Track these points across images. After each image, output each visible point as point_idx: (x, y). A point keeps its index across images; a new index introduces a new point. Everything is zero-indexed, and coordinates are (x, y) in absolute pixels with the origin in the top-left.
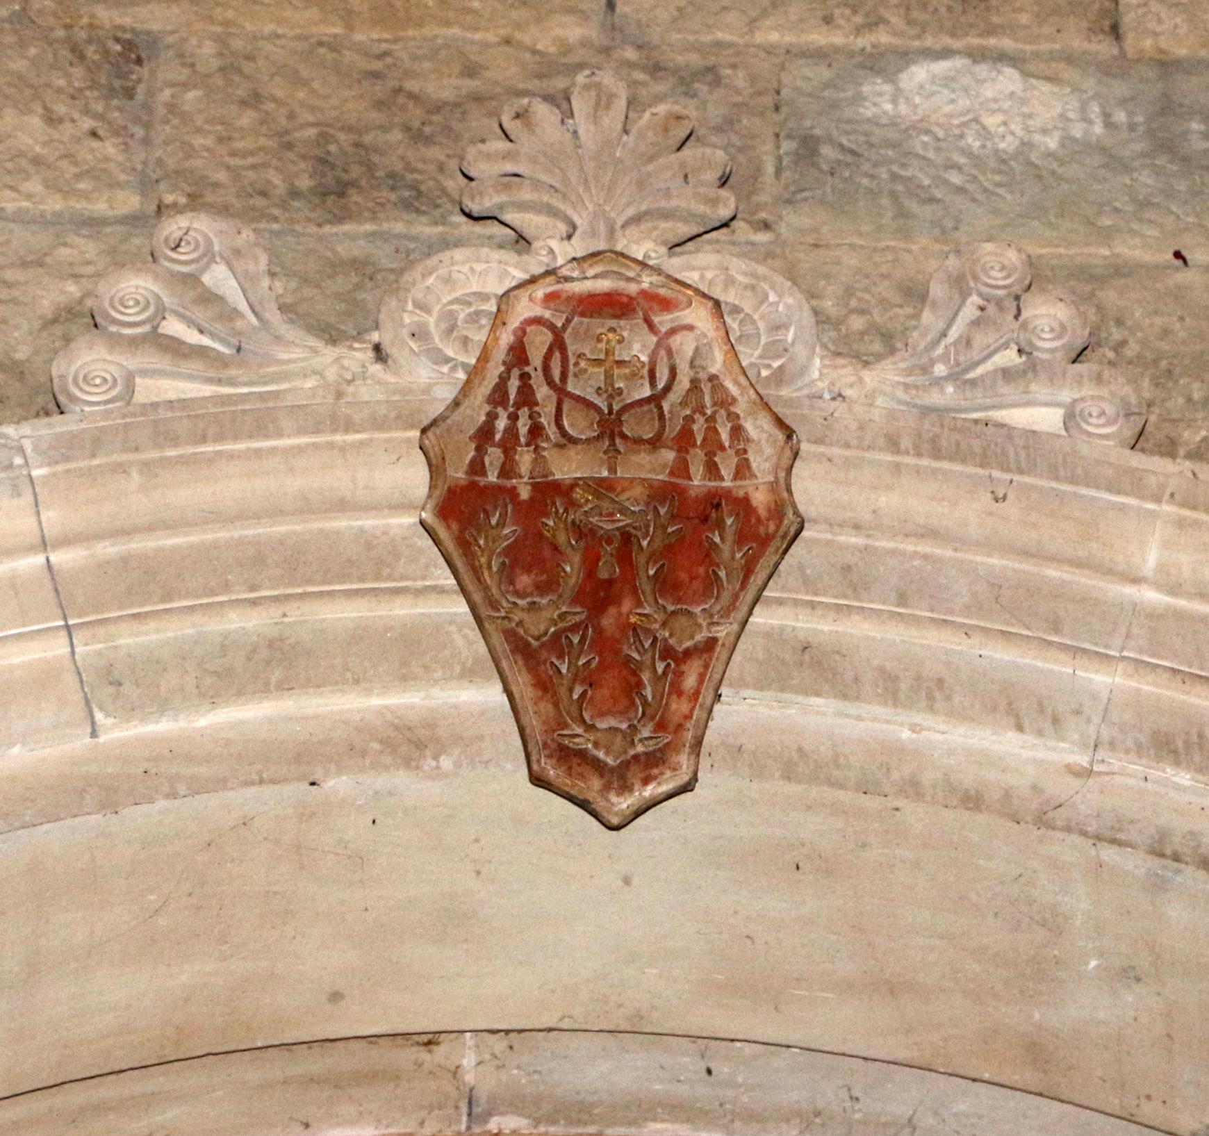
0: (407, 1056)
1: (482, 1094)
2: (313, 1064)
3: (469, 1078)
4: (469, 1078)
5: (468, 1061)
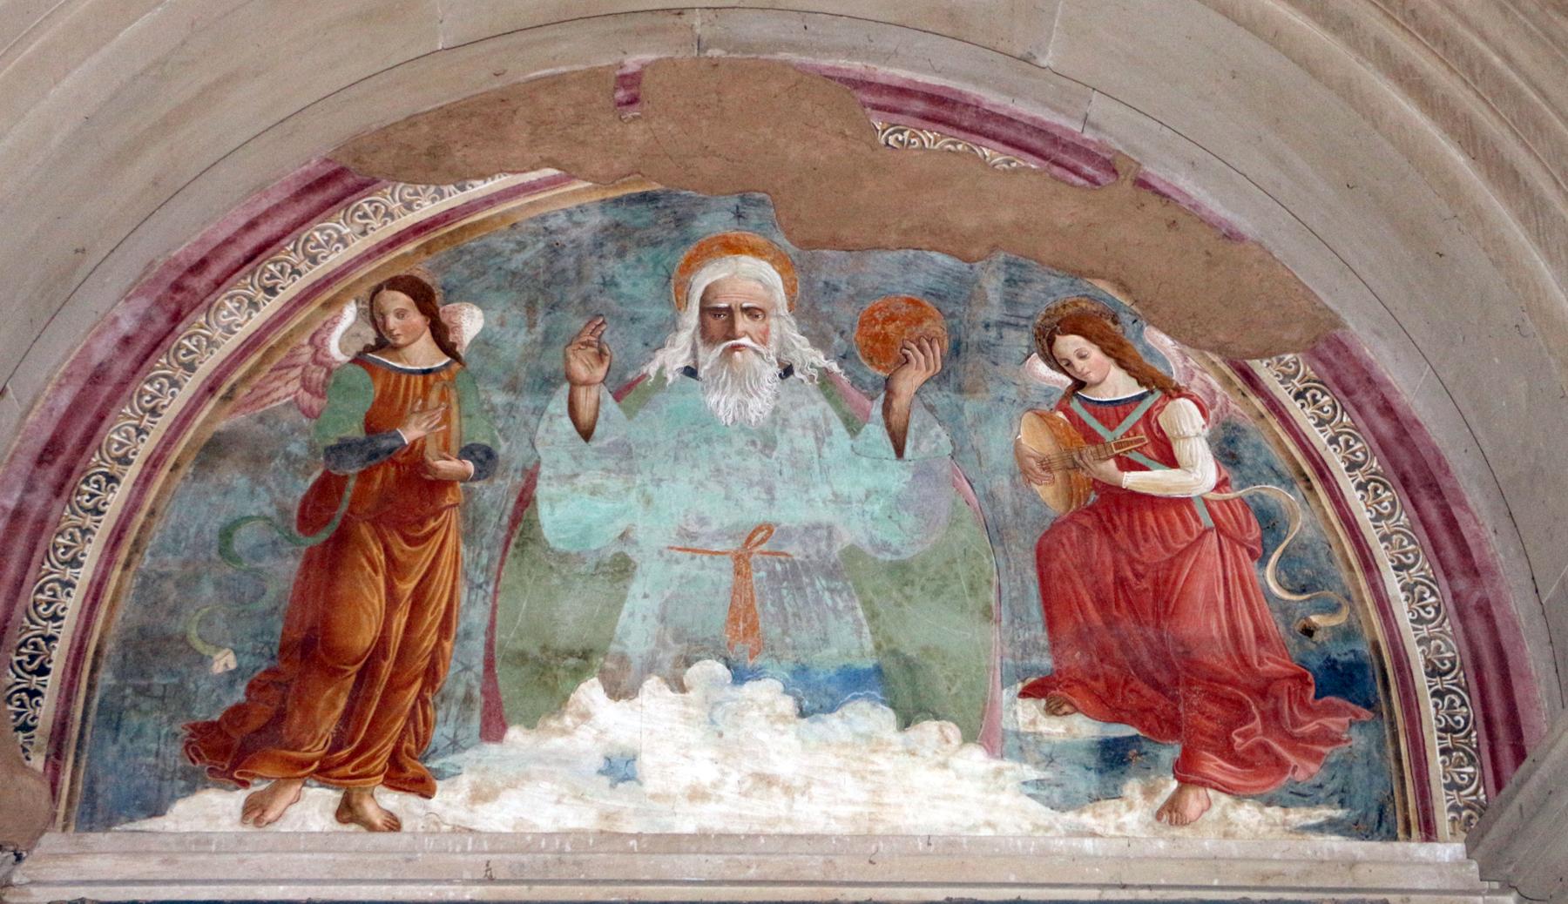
0: (671, 19)
1: (704, 39)
2: (629, 24)
3: (698, 31)
4: (698, 31)
5: (697, 23)
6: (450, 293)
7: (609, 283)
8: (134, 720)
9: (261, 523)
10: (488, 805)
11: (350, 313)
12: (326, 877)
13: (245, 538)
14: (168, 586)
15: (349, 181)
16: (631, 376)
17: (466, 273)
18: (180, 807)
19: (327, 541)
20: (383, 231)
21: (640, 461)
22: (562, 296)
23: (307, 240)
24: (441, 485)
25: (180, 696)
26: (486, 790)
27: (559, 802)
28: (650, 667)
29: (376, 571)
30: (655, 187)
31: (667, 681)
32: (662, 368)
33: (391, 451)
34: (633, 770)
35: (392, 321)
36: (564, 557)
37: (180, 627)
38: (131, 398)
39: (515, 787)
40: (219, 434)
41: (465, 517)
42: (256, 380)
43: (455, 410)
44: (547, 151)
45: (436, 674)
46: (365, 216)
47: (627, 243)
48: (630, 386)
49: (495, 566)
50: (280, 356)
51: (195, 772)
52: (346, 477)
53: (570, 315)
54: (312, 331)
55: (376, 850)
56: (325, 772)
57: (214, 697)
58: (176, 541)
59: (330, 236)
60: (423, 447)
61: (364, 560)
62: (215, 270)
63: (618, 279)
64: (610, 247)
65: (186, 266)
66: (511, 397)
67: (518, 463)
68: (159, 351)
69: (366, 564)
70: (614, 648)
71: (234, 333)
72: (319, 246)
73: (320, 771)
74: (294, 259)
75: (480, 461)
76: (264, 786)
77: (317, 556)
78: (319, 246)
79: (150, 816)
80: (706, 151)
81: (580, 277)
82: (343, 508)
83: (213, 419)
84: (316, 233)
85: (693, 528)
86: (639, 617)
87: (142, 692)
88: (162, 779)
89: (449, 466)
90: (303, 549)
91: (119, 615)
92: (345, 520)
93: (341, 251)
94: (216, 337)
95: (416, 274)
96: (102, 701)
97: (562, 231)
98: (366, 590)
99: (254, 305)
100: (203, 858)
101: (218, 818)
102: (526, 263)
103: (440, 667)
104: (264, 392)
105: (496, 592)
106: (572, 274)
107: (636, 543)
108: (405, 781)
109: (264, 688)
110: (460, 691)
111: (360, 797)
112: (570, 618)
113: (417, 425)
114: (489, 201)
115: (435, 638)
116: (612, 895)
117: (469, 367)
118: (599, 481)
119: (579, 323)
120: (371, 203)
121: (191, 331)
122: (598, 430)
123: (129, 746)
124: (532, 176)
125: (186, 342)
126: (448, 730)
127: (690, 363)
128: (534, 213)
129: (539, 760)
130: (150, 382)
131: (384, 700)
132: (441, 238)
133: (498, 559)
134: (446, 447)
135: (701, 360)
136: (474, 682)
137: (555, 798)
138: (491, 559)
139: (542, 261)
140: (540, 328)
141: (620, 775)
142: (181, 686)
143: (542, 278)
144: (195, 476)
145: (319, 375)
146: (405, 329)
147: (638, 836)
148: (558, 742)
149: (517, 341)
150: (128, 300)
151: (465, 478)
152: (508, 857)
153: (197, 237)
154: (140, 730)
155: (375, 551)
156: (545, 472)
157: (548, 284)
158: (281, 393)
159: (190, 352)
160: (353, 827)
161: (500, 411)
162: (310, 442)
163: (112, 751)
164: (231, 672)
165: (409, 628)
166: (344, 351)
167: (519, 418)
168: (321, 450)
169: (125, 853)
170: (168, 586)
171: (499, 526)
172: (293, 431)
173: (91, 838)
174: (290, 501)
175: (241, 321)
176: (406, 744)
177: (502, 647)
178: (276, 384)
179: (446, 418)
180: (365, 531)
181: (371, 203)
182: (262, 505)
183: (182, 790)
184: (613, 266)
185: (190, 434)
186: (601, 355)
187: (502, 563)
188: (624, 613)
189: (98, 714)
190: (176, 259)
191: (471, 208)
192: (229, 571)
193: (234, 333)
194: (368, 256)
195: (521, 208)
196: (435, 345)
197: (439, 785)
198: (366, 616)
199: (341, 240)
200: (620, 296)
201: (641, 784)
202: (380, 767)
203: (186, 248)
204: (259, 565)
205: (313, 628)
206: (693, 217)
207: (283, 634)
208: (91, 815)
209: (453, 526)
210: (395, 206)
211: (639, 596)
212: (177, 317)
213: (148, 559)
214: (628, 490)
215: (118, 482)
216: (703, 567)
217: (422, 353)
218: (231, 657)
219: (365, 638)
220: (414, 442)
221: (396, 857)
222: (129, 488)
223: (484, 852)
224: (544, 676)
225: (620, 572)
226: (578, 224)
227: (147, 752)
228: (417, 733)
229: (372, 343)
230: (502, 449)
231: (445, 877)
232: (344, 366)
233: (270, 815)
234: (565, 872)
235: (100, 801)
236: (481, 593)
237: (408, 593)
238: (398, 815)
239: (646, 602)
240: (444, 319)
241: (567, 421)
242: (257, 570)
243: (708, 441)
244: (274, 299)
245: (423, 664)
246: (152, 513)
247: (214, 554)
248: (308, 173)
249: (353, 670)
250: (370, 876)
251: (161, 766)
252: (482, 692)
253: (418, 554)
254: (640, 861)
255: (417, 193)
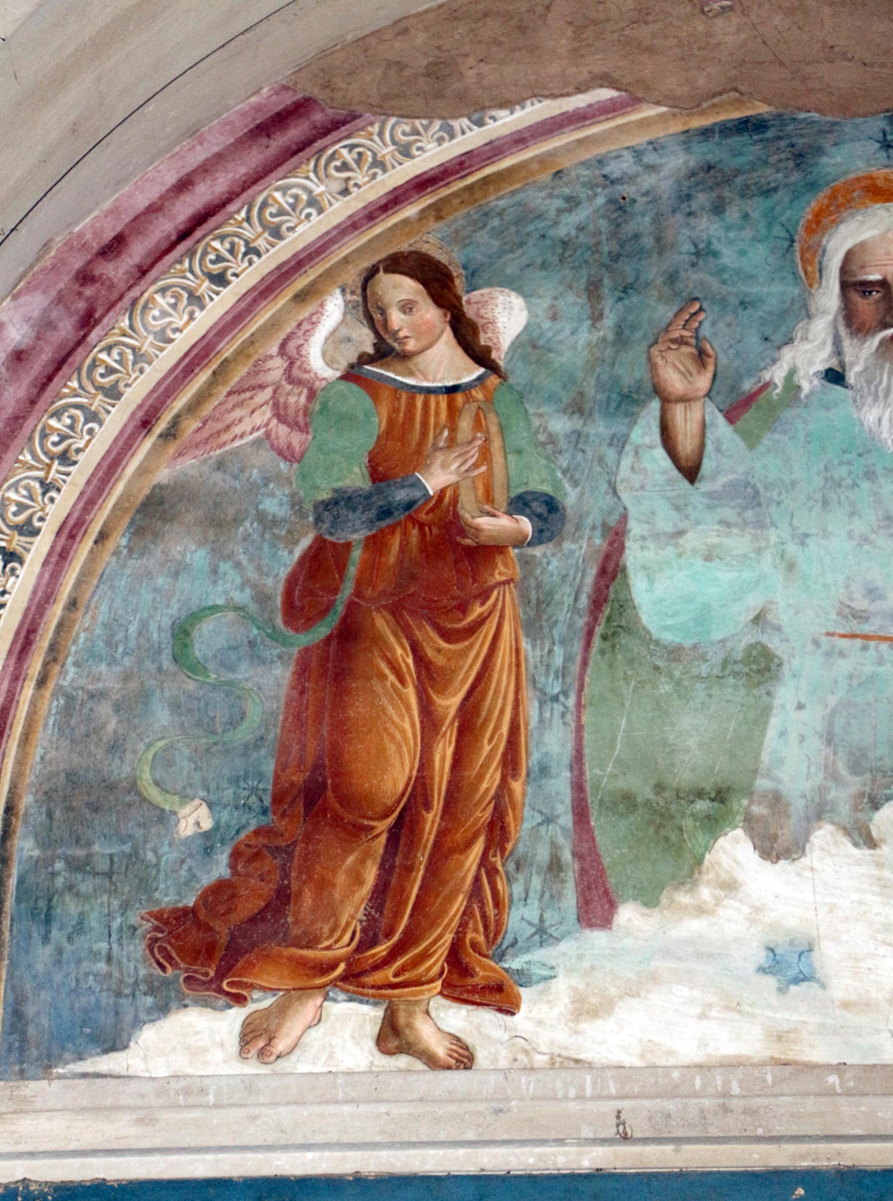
6: (476, 276)
7: (703, 253)
8: (71, 908)
9: (231, 615)
10: (599, 1023)
11: (334, 308)
12: (379, 1139)
13: (209, 637)
14: (104, 710)
15: (318, 117)
16: (748, 386)
17: (496, 244)
18: (149, 1036)
19: (328, 640)
20: (373, 188)
21: (773, 509)
22: (638, 273)
23: (264, 205)
24: (486, 553)
25: (133, 870)
26: (594, 1000)
27: (703, 1016)
28: (820, 811)
29: (402, 681)
30: (761, 109)
31: (847, 832)
32: (793, 372)
33: (410, 505)
34: (810, 965)
35: (396, 318)
36: (675, 653)
37: (127, 769)
38: (31, 439)
39: (638, 995)
40: (159, 487)
41: (526, 599)
42: (207, 409)
43: (496, 443)
44: (595, 63)
45: (504, 829)
46: (345, 167)
47: (726, 193)
48: (749, 400)
49: (575, 668)
50: (240, 372)
51: (166, 983)
52: (348, 546)
53: (652, 301)
54: (282, 336)
55: (451, 1098)
56: (355, 979)
57: (183, 873)
58: (110, 643)
59: (296, 197)
60: (455, 500)
61: (383, 666)
62: (137, 251)
63: (716, 246)
64: (702, 199)
65: (96, 246)
66: (577, 423)
67: (594, 517)
68: (65, 369)
69: (387, 671)
70: (762, 784)
71: (171, 341)
72: (281, 212)
73: (345, 978)
74: (248, 233)
75: (539, 516)
76: (268, 1002)
77: (314, 662)
78: (281, 212)
79: (106, 1051)
80: (830, 53)
81: (662, 246)
82: (347, 590)
83: (152, 466)
84: (277, 193)
85: (861, 604)
86: (793, 738)
87: (78, 866)
88: (119, 994)
89: (495, 524)
90: (295, 651)
91: (37, 752)
92: (351, 607)
93: (314, 218)
94: (146, 347)
95: (425, 248)
96: (21, 881)
97: (631, 179)
98: (390, 710)
99: (196, 300)
100: (196, 1114)
101: (205, 1050)
102: (581, 228)
103: (510, 818)
104: (220, 426)
105: (579, 705)
106: (648, 241)
107: (778, 629)
108: (474, 990)
109: (257, 856)
110: (543, 854)
111: (411, 1014)
112: (692, 742)
113: (444, 466)
114: (520, 139)
115: (498, 776)
116: (803, 1157)
117: (511, 380)
118: (716, 540)
119: (664, 312)
120: (351, 147)
121: (110, 340)
122: (707, 466)
123: (68, 947)
124: (579, 101)
125: (103, 356)
126: (531, 912)
127: (833, 363)
128: (587, 155)
129: (667, 953)
130: (57, 414)
131: (433, 868)
132: (455, 195)
133: (579, 659)
134: (489, 497)
135: (848, 359)
136: (561, 840)
137: (699, 1010)
138: (568, 658)
139: (603, 224)
140: (609, 321)
141: (792, 973)
142: (134, 856)
143: (606, 249)
144: (130, 550)
145: (297, 399)
146: (414, 327)
147: (840, 1068)
148: (694, 926)
149: (577, 341)
150: (15, 297)
151: (520, 542)
152: (647, 1103)
153: (107, 205)
154: (80, 923)
155: (399, 651)
156: (635, 528)
157: (615, 257)
158: (246, 426)
159: (110, 371)
160: (403, 1061)
161: (563, 444)
162: (293, 495)
163: (43, 954)
164: (206, 835)
165: (457, 762)
166: (330, 362)
167: (590, 454)
168: (308, 507)
169: (83, 1109)
170: (104, 710)
171: (574, 609)
172: (266, 481)
173: (32, 1087)
174: (270, 581)
175: (180, 324)
176: (470, 936)
177: (597, 787)
178: (237, 413)
179: (485, 455)
180: (382, 623)
181: (351, 147)
182: (230, 588)
183: (149, 1011)
184: (707, 227)
185: (119, 488)
186: (701, 357)
187: (585, 663)
188: (771, 733)
189: (19, 900)
190: (80, 235)
191: (494, 150)
192: (191, 686)
193: (171, 341)
194: (353, 225)
195: (568, 149)
196: (460, 352)
197: (525, 993)
198: (394, 752)
199: (312, 202)
200: (724, 269)
201: (823, 986)
202: (436, 970)
203: (95, 221)
204: (231, 676)
205: (318, 767)
206: (820, 151)
207: (277, 777)
208: (22, 1050)
209: (508, 612)
210: (387, 151)
211: (791, 706)
212: (88, 321)
213: (72, 671)
214: (759, 551)
215: (21, 562)
216: (880, 661)
217: (442, 363)
218: (204, 810)
219: (394, 778)
220: (443, 491)
221: (481, 1107)
222: (37, 568)
223: (610, 1097)
224: (664, 828)
225: (759, 672)
226: (652, 168)
227: (95, 956)
228: (484, 917)
229: (370, 350)
230: (570, 497)
231: (554, 1135)
232: (330, 385)
233: (281, 1045)
234: (733, 1125)
235: (31, 1031)
236: (558, 708)
237: (453, 711)
238: (469, 1040)
239: (804, 715)
240: (470, 312)
241: (660, 453)
242: (231, 684)
243: (870, 475)
244: (224, 291)
245: (484, 815)
246: (73, 604)
247: (166, 662)
248: (258, 108)
249: (383, 826)
250: (442, 1137)
251: (116, 974)
252: (574, 854)
253: (463, 654)
254: (846, 1106)
255: (415, 132)
